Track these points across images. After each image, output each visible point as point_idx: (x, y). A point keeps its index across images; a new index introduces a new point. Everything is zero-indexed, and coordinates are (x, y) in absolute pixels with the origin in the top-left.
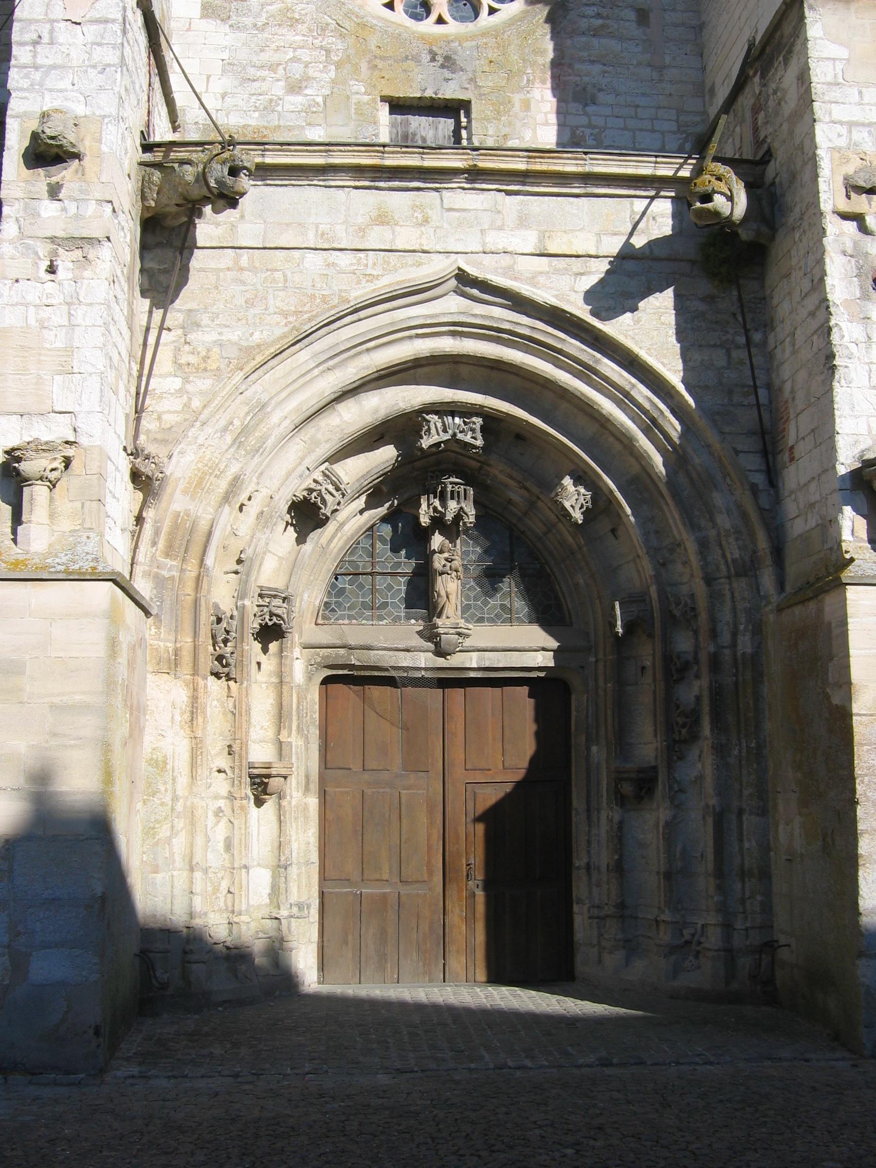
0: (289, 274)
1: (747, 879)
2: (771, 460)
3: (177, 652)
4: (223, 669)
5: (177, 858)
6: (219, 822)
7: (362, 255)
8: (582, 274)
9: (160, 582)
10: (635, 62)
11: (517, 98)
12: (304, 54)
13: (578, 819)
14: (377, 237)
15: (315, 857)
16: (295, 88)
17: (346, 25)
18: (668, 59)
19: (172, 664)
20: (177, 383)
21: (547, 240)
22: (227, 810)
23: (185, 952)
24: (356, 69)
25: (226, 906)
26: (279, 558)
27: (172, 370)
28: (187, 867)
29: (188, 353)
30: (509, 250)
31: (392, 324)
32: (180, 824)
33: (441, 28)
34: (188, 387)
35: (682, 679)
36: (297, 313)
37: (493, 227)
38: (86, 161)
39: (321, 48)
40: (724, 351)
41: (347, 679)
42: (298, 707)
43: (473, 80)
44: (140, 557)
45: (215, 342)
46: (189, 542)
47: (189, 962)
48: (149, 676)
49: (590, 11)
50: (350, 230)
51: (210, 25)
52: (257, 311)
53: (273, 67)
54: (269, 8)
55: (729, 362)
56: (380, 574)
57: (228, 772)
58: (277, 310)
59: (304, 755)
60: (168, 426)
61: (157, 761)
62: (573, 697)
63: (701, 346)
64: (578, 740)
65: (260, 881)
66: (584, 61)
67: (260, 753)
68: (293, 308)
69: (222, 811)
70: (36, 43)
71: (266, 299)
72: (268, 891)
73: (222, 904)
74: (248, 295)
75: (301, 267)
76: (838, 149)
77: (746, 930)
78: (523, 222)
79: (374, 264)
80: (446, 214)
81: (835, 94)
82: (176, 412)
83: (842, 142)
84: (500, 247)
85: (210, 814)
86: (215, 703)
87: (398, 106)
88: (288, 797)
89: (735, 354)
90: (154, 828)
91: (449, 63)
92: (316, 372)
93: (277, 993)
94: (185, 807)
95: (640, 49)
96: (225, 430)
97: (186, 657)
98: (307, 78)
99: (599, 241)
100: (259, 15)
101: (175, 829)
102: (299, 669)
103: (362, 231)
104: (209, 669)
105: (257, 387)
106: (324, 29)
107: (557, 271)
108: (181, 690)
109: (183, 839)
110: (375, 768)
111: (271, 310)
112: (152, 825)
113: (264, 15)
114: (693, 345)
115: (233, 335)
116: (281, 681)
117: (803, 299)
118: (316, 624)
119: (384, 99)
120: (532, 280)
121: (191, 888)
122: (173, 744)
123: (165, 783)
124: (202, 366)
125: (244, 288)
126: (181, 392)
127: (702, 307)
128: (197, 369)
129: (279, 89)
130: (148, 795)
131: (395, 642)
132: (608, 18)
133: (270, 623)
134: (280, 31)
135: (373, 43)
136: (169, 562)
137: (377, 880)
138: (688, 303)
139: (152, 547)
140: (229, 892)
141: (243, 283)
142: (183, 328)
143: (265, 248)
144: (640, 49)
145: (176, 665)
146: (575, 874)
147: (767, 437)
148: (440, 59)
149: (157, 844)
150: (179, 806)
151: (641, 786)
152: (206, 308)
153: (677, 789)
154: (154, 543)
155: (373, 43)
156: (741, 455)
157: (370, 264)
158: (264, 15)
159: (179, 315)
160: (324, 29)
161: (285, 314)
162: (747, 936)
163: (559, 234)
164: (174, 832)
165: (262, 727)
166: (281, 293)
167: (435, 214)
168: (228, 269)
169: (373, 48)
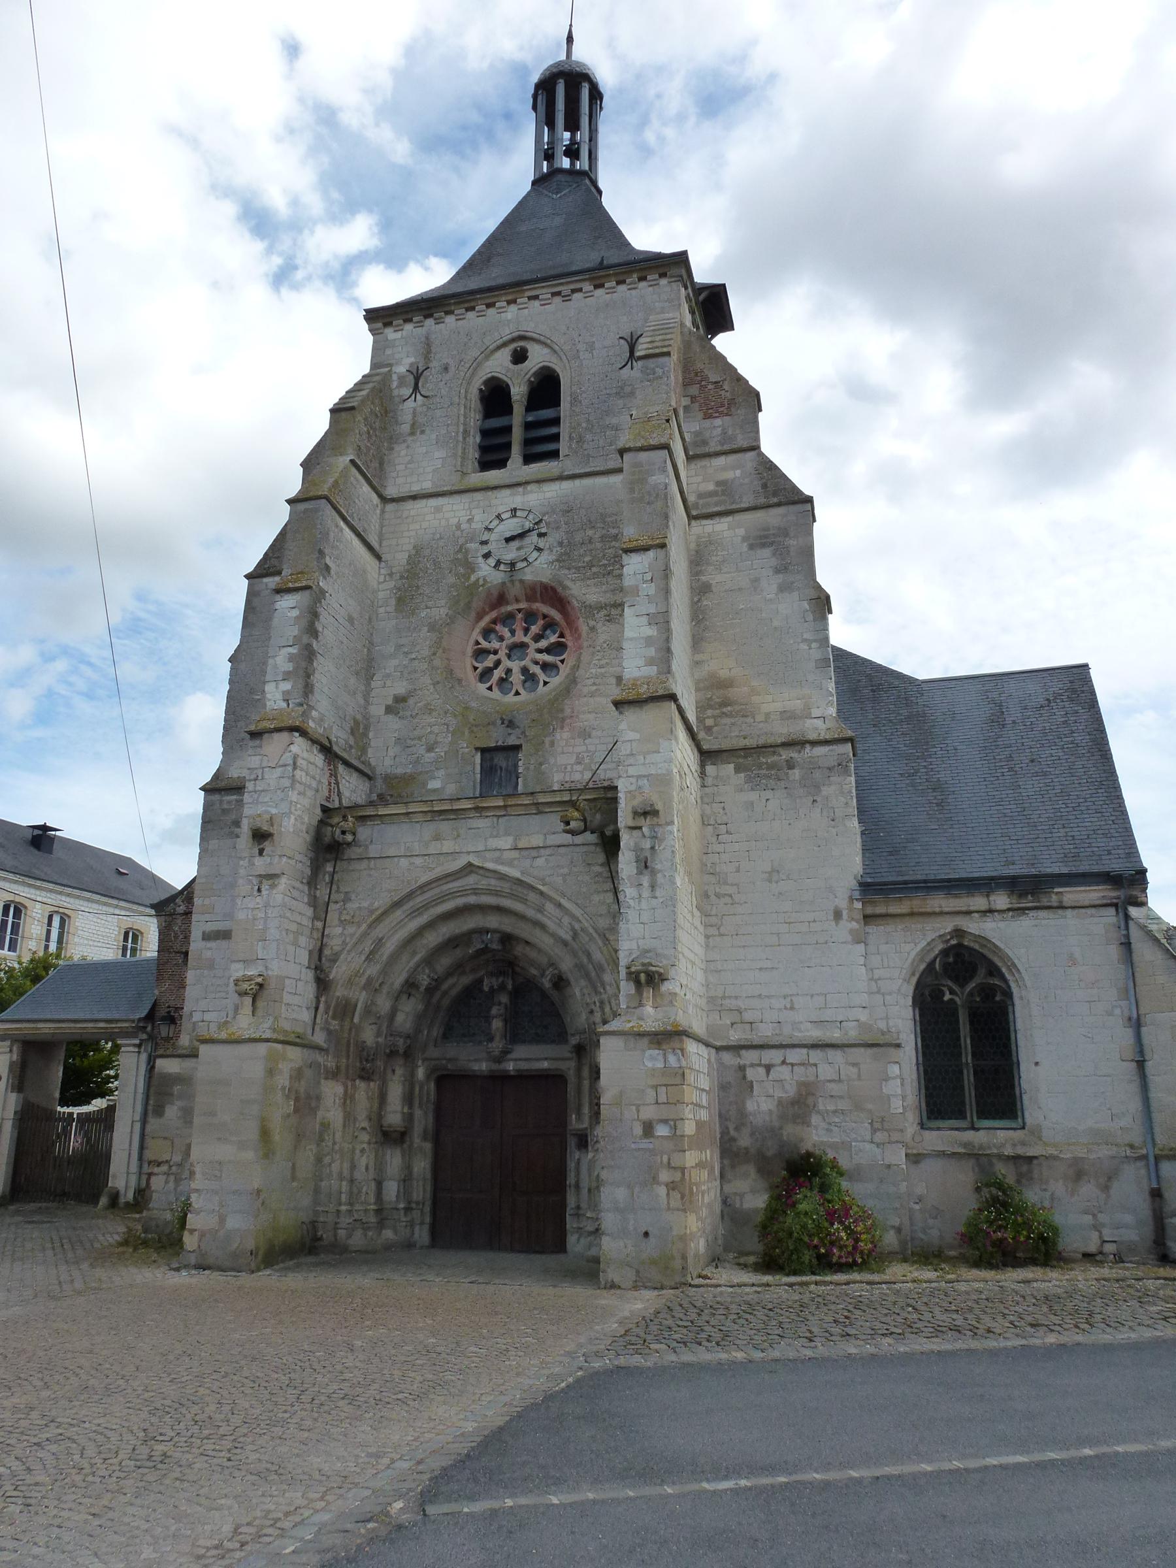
3: (338, 1067)
9: (330, 1032)
11: (547, 740)
12: (436, 729)
15: (429, 1176)
16: (430, 749)
19: (333, 1075)
20: (339, 930)
24: (463, 733)
33: (517, 698)
38: (275, 837)
41: (448, 1081)
43: (523, 733)
44: (318, 1021)
46: (345, 1010)
49: (590, 682)
51: (390, 717)
53: (420, 738)
59: (423, 1120)
65: (391, 1189)
67: (394, 1117)
70: (255, 780)
76: (630, 792)
81: (631, 761)
83: (633, 788)
85: (357, 1152)
87: (484, 751)
91: (511, 724)
97: (343, 1068)
98: (436, 743)
102: (421, 1073)
105: (377, 930)
115: (365, 904)
116: (410, 1081)
119: (477, 749)
129: (422, 751)
131: (476, 1060)
135: (471, 718)
148: (506, 722)
150: (337, 1147)
155: (471, 718)
161: (389, 891)
164: (333, 1161)
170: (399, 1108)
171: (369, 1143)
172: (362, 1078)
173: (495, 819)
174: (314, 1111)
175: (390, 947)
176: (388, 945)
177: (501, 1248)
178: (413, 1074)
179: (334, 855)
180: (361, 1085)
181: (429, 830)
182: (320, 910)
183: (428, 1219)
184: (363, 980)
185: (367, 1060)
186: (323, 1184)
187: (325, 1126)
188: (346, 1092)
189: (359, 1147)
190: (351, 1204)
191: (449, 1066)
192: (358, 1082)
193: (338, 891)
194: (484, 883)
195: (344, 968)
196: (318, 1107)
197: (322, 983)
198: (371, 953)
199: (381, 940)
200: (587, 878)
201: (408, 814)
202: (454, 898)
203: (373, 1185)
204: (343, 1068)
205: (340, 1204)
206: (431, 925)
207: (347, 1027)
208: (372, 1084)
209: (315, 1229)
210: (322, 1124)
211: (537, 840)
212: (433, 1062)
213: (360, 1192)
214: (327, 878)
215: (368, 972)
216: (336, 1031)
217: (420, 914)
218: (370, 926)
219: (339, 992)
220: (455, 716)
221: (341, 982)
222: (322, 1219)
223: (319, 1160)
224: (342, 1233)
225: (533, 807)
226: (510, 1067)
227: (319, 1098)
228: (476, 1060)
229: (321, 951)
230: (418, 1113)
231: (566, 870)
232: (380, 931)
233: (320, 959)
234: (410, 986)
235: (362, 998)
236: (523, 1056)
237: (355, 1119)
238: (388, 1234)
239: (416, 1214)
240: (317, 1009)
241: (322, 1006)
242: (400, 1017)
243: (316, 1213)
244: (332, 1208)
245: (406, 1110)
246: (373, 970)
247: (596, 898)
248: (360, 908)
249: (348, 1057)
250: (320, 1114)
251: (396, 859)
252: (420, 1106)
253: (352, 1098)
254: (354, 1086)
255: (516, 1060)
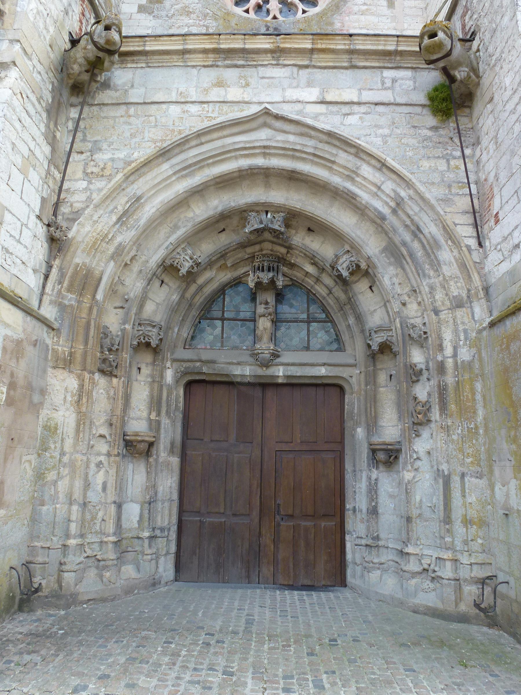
0: (158, 117)
1: (469, 526)
2: (479, 230)
3: (71, 354)
4: (108, 370)
5: (61, 496)
6: (99, 471)
7: (206, 106)
8: (348, 114)
9: (62, 308)
10: (386, 28)
13: (348, 476)
14: (215, 94)
15: (175, 496)
17: (219, 14)
18: (406, 26)
19: (66, 363)
20: (83, 184)
21: (325, 94)
22: (106, 463)
23: (61, 564)
25: (101, 530)
26: (157, 304)
27: (82, 176)
28: (68, 502)
29: (93, 166)
30: (301, 99)
31: (223, 146)
32: (65, 471)
34: (92, 187)
35: (418, 381)
36: (162, 140)
37: (290, 86)
39: (204, 25)
40: (445, 160)
41: (195, 385)
42: (167, 399)
44: (48, 289)
45: (110, 159)
46: (84, 282)
47: (63, 571)
48: (50, 370)
50: (199, 90)
52: (137, 140)
54: (176, 6)
55: (449, 168)
56: (229, 319)
57: (108, 437)
58: (416, 480)
59: (170, 431)
60: (76, 210)
61: (50, 427)
62: (346, 396)
63: (429, 157)
64: (348, 424)
65: (133, 512)
66: (356, 28)
67: (138, 425)
68: (160, 138)
69: (102, 464)
71: (143, 132)
72: (138, 518)
73: (98, 528)
74: (132, 131)
75: (167, 113)
77: (471, 564)
78: (310, 84)
79: (213, 111)
80: (261, 81)
82: (82, 202)
84: (295, 98)
85: (92, 466)
86: (102, 391)
88: (155, 456)
89: (452, 163)
90: (44, 474)
92: (174, 178)
93: (136, 592)
94: (70, 460)
95: (389, 20)
96: (112, 212)
97: (78, 357)
99: (360, 94)
100: (170, 10)
101: (61, 474)
102: (169, 376)
103: (206, 91)
104: (97, 368)
105: (135, 186)
106: (205, 16)
107: (332, 113)
108: (73, 380)
109: (67, 482)
110: (218, 439)
111: (146, 139)
112: (42, 471)
113: (173, 10)
114: (424, 157)
116: (157, 381)
117: (504, 107)
118: (184, 348)
120: (316, 117)
121: (69, 517)
122: (64, 416)
123: (55, 442)
124: (101, 174)
125: (130, 127)
126: (86, 189)
127: (429, 133)
128: (97, 176)
130: (42, 450)
132: (370, 5)
133: (143, 341)
134: (181, 18)
136: (70, 296)
137: (217, 513)
138: (420, 131)
139: (59, 285)
140: (103, 520)
141: (130, 124)
142: (91, 151)
143: (145, 103)
144: (389, 20)
145: (70, 363)
146: (346, 513)
147: (477, 215)
149: (44, 485)
150: (66, 459)
151: (388, 457)
152: (106, 139)
153: (415, 457)
154: (60, 283)
156: (458, 226)
157: (210, 110)
158: (173, 10)
159: (89, 144)
160: (205, 16)
162: (471, 570)
163: (333, 90)
164: (60, 477)
165: (139, 410)
166: (153, 130)
167: (253, 81)
168: (122, 116)
169: (233, 25)
170: (145, 414)
171: (109, 455)
172: (102, 372)
173: (295, 69)
174: (36, 408)
175: (149, 210)
176: (147, 208)
177: (260, 581)
178: (162, 376)
179: (81, 100)
180: (101, 381)
181: (208, 76)
182: (61, 161)
183: (173, 548)
184: (111, 249)
185: (110, 350)
186: (45, 508)
187: (51, 430)
188: (81, 386)
189: (94, 460)
190: (82, 536)
191: (205, 370)
192: (97, 376)
193: (84, 140)
194: (280, 139)
195: (88, 228)
196: (42, 404)
197: (56, 243)
198: (125, 213)
199: (139, 199)
200: (413, 142)
201: (184, 52)
202: (236, 158)
203: (113, 509)
204: (78, 357)
205: (68, 536)
206: (199, 192)
207: (86, 305)
208: (115, 380)
209: (30, 575)
210: (46, 428)
211: (351, 95)
212: (185, 365)
213: (94, 518)
214: (71, 125)
215: (119, 239)
216: (71, 306)
217: (191, 174)
218: (127, 177)
219: (79, 258)
220: (216, 19)
221: (82, 246)
222: (40, 559)
223: (39, 476)
224: (69, 577)
225: (345, 57)
226: (280, 372)
227: (43, 392)
228: (239, 364)
229: (57, 206)
230: (165, 422)
231: (386, 131)
232: (141, 186)
233: (55, 214)
234: (168, 268)
235: (109, 270)
236: (290, 361)
237: (91, 423)
238: (129, 571)
239: (161, 543)
240: (46, 277)
241: (54, 272)
242: (149, 308)
243: (32, 549)
244: (56, 542)
245: (153, 416)
246: (126, 236)
247: (426, 164)
248: (113, 160)
249: (86, 343)
250: (44, 413)
251: (164, 106)
252: (168, 413)
253: (89, 394)
254: (91, 379)
255: (288, 365)
